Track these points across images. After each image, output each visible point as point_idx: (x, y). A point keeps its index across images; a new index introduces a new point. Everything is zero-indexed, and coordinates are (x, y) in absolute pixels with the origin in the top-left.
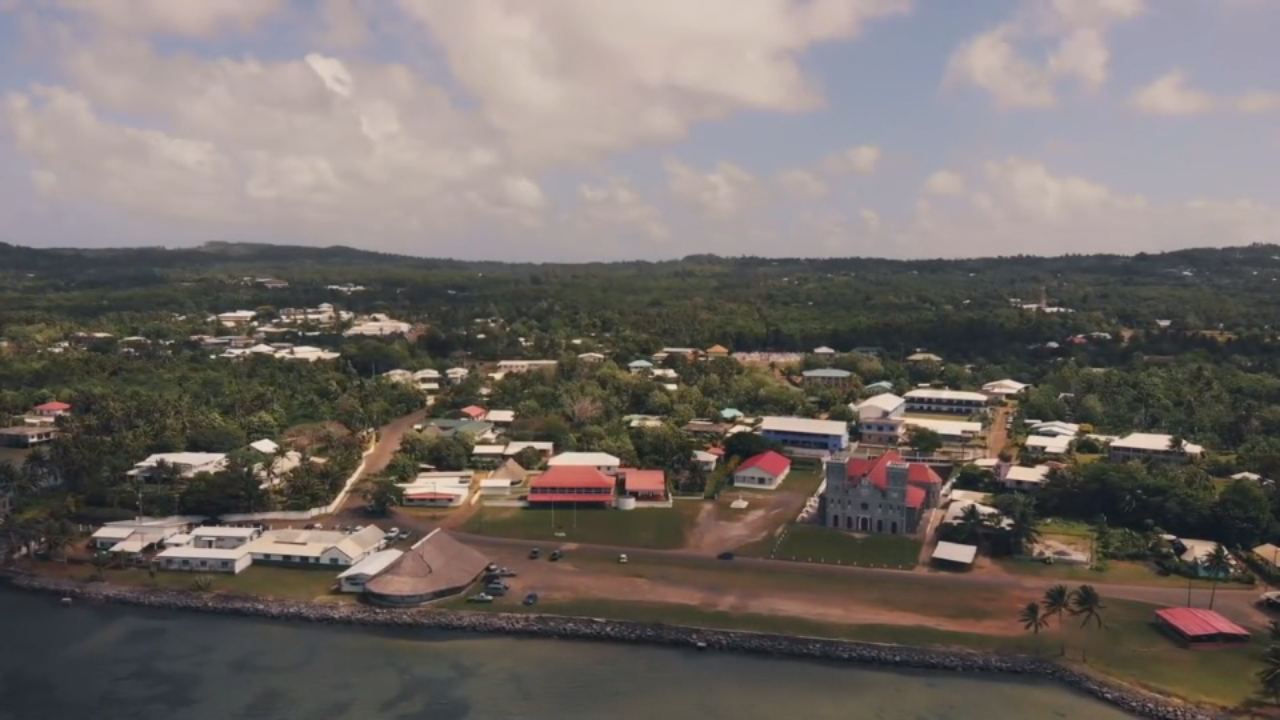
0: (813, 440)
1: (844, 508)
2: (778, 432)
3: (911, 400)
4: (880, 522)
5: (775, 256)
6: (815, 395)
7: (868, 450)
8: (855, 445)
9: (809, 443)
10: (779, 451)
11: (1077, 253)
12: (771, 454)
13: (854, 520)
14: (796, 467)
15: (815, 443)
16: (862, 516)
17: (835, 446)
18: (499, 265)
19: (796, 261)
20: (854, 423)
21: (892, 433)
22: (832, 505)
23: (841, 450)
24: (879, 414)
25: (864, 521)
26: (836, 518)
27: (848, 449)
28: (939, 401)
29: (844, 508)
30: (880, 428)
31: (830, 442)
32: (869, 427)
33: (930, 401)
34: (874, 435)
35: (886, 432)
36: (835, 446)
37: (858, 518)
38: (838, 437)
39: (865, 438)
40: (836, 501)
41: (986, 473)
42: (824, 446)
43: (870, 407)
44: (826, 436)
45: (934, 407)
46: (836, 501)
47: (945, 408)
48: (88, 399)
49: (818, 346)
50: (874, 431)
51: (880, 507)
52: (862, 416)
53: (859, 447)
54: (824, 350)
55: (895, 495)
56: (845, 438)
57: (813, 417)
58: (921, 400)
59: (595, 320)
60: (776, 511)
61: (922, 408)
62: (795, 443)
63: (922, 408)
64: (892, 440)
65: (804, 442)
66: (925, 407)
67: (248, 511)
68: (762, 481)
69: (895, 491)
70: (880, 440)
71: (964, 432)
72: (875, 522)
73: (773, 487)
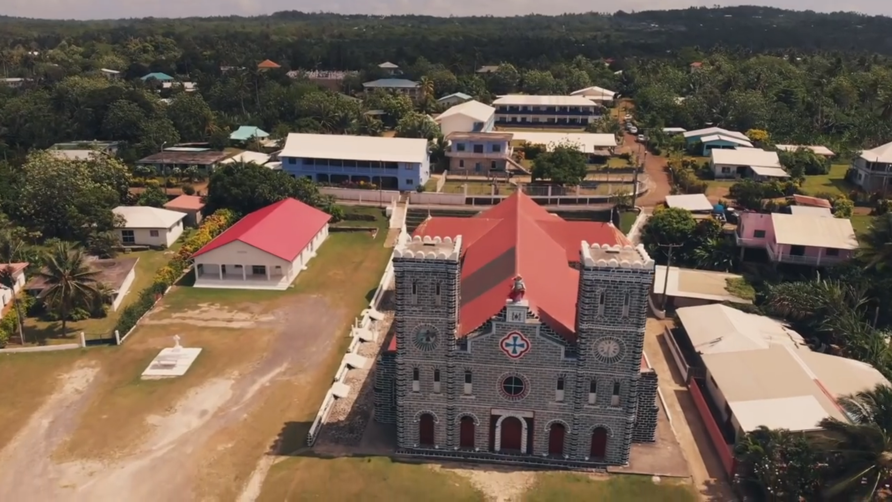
0: (371, 173)
1: (451, 391)
2: (309, 161)
3: (501, 109)
4: (558, 429)
5: (348, 14)
6: (375, 107)
7: (465, 186)
8: (441, 179)
9: (366, 179)
10: (307, 198)
11: (572, 13)
12: (292, 205)
13: (481, 426)
14: (342, 224)
15: (376, 180)
16: (505, 414)
17: (409, 182)
18: (123, 20)
19: (365, 17)
20: (435, 140)
21: (494, 156)
22: (416, 385)
23: (420, 189)
24: (471, 127)
25: (512, 425)
26: (427, 421)
27: (432, 186)
28: (537, 110)
29: (451, 391)
30: (478, 149)
31: (402, 177)
32: (460, 147)
33: (525, 109)
34: (470, 159)
35: (488, 155)
36: (409, 182)
37: (494, 418)
38: (413, 167)
39: (455, 165)
40: (427, 373)
41: (705, 228)
42: (392, 184)
43: (459, 115)
44: (394, 165)
45: (530, 118)
46: (427, 373)
47: (543, 118)
48: (420, 127)
49: (383, 62)
50: (468, 154)
51: (560, 386)
52: (446, 131)
53: (447, 180)
54: (387, 65)
55: (609, 348)
56: (425, 167)
57: (374, 134)
58: (514, 109)
59: (147, 44)
60: (265, 380)
61: (514, 119)
62: (339, 181)
63: (514, 119)
64: (497, 167)
65: (355, 179)
66: (519, 118)
67: (578, 89)
68: (259, 272)
69: (607, 336)
70: (478, 169)
71: (597, 148)
72: (544, 429)
73: (283, 285)
